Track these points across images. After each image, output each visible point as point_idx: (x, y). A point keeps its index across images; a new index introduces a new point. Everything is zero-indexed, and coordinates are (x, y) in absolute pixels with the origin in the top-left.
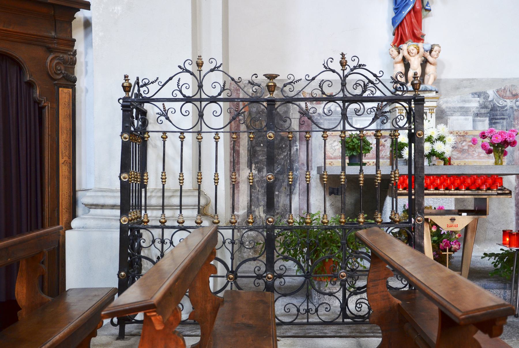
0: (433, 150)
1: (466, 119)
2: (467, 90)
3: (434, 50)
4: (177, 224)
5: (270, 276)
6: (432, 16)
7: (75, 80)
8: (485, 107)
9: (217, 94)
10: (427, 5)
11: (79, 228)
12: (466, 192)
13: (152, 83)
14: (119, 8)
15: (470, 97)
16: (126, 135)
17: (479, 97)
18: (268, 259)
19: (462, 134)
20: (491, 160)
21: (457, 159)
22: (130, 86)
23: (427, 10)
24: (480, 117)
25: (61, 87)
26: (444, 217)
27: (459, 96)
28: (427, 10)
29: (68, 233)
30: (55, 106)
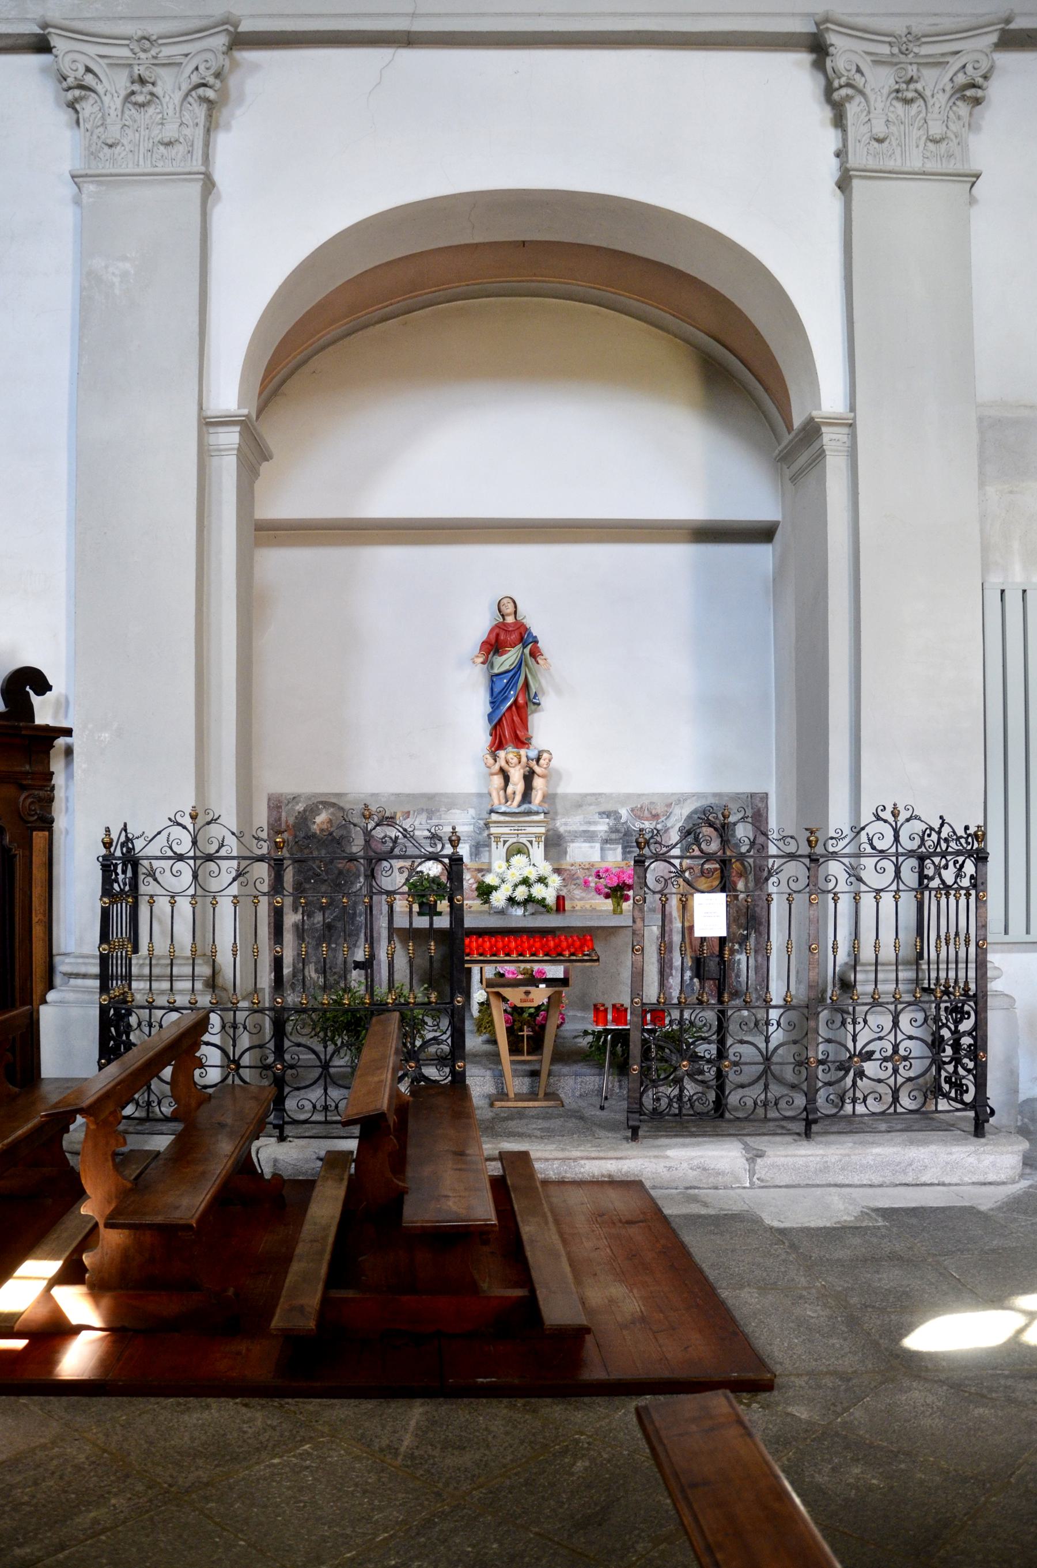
0: (530, 896)
1: (591, 847)
2: (592, 807)
3: (543, 758)
4: (167, 1004)
5: (279, 1066)
6: (543, 710)
7: (52, 821)
8: (617, 831)
9: (214, 851)
10: (534, 698)
11: (55, 1002)
12: (546, 958)
13: (137, 838)
14: (107, 735)
15: (596, 817)
16: (106, 900)
17: (608, 817)
18: (276, 1046)
19: (587, 867)
20: (608, 904)
21: (581, 899)
22: (111, 844)
23: (534, 704)
24: (610, 844)
25: (35, 830)
26: (516, 989)
27: (582, 817)
28: (534, 704)
29: (43, 1009)
30: (27, 853)
